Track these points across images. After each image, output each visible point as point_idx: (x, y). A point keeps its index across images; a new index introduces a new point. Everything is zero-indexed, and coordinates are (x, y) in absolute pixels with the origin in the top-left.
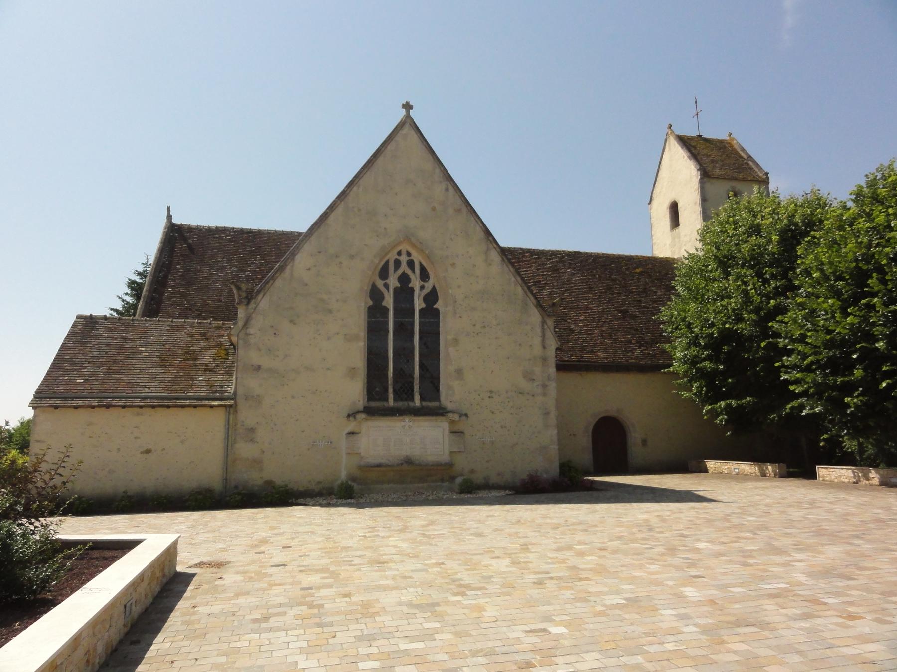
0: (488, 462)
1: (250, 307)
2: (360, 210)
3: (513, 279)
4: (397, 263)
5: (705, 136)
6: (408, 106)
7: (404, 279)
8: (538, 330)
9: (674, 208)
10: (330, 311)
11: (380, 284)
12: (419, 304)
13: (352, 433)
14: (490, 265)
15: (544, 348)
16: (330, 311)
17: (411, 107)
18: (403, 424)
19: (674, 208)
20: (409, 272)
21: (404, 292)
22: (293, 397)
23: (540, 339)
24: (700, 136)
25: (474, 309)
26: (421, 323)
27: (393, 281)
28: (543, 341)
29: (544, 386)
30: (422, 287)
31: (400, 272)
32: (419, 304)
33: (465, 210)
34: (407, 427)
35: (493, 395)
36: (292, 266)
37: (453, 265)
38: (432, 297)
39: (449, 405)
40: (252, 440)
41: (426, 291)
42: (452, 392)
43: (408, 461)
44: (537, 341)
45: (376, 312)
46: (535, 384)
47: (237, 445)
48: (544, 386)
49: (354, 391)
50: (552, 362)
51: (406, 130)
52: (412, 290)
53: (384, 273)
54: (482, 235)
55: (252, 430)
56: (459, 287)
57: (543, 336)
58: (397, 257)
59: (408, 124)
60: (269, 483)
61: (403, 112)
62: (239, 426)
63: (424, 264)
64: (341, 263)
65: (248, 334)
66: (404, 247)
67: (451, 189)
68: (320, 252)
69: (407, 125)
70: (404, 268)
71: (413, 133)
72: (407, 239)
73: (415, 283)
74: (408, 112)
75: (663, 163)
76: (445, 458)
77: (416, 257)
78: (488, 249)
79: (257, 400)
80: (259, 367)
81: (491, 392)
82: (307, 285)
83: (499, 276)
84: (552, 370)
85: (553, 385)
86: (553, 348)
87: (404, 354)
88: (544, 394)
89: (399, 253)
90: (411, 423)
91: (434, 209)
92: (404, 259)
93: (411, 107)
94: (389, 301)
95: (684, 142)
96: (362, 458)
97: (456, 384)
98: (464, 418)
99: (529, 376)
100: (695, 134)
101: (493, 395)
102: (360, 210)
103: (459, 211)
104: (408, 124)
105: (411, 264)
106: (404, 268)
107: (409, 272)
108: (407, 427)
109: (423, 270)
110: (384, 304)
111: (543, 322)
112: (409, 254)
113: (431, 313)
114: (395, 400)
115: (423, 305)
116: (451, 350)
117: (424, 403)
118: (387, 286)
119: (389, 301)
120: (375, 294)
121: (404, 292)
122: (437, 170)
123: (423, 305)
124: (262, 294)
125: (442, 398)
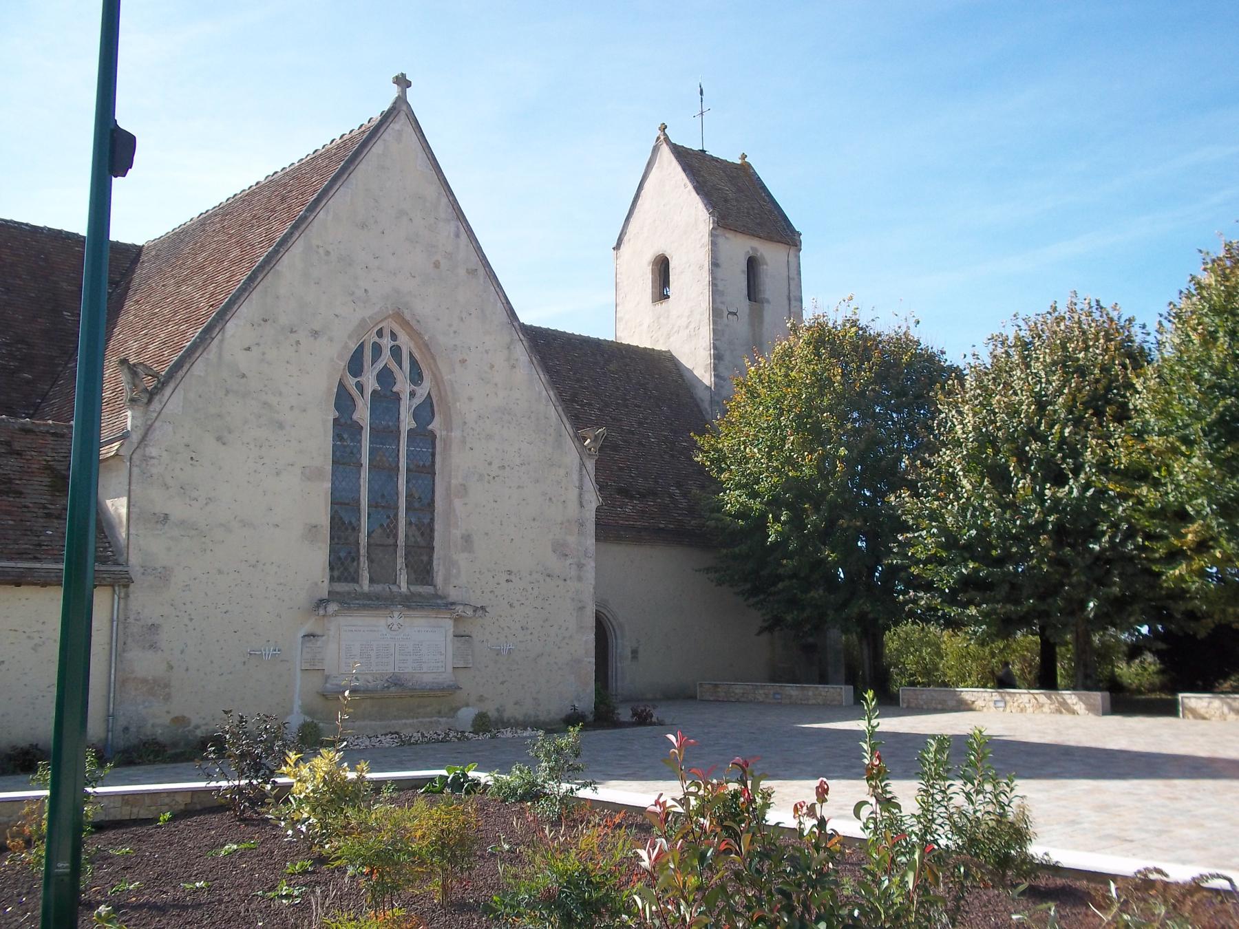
0: (502, 683)
1: (152, 408)
2: (328, 253)
3: (544, 393)
4: (377, 349)
5: (711, 151)
6: (402, 82)
7: (385, 377)
8: (575, 476)
9: (662, 268)
10: (281, 426)
11: (351, 382)
12: (407, 422)
13: (310, 636)
14: (513, 367)
15: (582, 506)
16: (281, 426)
17: (409, 84)
18: (390, 620)
19: (662, 268)
20: (394, 366)
21: (386, 400)
22: (220, 572)
23: (576, 491)
24: (703, 151)
25: (489, 437)
26: (409, 455)
27: (370, 381)
28: (580, 495)
29: (580, 566)
30: (412, 394)
31: (380, 365)
32: (407, 422)
33: (481, 271)
34: (395, 627)
35: (512, 577)
36: (222, 341)
37: (463, 361)
38: (425, 411)
39: (453, 595)
40: (153, 646)
41: (417, 401)
42: (458, 571)
43: (396, 681)
44: (573, 494)
45: (344, 429)
46: (569, 561)
47: (128, 655)
48: (580, 566)
49: (314, 562)
50: (591, 527)
51: (400, 124)
52: (397, 398)
53: (355, 365)
54: (504, 318)
55: (154, 628)
56: (470, 399)
57: (581, 487)
58: (376, 339)
59: (399, 111)
60: (180, 721)
61: (394, 91)
62: (131, 620)
63: (417, 356)
64: (298, 342)
65: (146, 459)
66: (388, 325)
67: (464, 236)
68: (265, 321)
69: (402, 116)
70: (386, 358)
71: (409, 129)
72: (398, 316)
73: (403, 385)
74: (404, 93)
75: (647, 185)
76: (446, 677)
77: (404, 340)
78: (512, 341)
79: (163, 576)
80: (166, 517)
81: (510, 573)
82: (244, 376)
83: (527, 386)
84: (591, 541)
85: (591, 565)
86: (594, 506)
87: (383, 504)
88: (580, 579)
89: (380, 333)
90: (401, 621)
91: (437, 265)
92: (386, 342)
93: (409, 84)
94: (363, 414)
95: (684, 156)
96: (327, 678)
97: (461, 558)
98: (480, 613)
99: (560, 549)
100: (696, 146)
101: (512, 577)
102: (328, 253)
103: (472, 272)
104: (399, 111)
105: (396, 352)
106: (386, 358)
107: (394, 366)
108: (395, 627)
109: (414, 362)
110: (355, 417)
111: (582, 465)
112: (394, 336)
113: (424, 437)
114: (371, 581)
115: (413, 425)
116: (457, 503)
117: (412, 588)
118: (360, 387)
119: (363, 414)
120: (344, 401)
121: (386, 400)
122: (444, 200)
123: (413, 425)
124: (172, 385)
125: (439, 580)
